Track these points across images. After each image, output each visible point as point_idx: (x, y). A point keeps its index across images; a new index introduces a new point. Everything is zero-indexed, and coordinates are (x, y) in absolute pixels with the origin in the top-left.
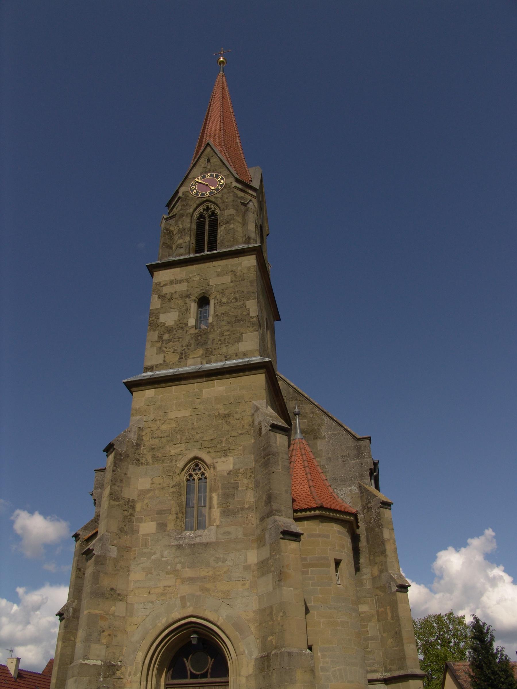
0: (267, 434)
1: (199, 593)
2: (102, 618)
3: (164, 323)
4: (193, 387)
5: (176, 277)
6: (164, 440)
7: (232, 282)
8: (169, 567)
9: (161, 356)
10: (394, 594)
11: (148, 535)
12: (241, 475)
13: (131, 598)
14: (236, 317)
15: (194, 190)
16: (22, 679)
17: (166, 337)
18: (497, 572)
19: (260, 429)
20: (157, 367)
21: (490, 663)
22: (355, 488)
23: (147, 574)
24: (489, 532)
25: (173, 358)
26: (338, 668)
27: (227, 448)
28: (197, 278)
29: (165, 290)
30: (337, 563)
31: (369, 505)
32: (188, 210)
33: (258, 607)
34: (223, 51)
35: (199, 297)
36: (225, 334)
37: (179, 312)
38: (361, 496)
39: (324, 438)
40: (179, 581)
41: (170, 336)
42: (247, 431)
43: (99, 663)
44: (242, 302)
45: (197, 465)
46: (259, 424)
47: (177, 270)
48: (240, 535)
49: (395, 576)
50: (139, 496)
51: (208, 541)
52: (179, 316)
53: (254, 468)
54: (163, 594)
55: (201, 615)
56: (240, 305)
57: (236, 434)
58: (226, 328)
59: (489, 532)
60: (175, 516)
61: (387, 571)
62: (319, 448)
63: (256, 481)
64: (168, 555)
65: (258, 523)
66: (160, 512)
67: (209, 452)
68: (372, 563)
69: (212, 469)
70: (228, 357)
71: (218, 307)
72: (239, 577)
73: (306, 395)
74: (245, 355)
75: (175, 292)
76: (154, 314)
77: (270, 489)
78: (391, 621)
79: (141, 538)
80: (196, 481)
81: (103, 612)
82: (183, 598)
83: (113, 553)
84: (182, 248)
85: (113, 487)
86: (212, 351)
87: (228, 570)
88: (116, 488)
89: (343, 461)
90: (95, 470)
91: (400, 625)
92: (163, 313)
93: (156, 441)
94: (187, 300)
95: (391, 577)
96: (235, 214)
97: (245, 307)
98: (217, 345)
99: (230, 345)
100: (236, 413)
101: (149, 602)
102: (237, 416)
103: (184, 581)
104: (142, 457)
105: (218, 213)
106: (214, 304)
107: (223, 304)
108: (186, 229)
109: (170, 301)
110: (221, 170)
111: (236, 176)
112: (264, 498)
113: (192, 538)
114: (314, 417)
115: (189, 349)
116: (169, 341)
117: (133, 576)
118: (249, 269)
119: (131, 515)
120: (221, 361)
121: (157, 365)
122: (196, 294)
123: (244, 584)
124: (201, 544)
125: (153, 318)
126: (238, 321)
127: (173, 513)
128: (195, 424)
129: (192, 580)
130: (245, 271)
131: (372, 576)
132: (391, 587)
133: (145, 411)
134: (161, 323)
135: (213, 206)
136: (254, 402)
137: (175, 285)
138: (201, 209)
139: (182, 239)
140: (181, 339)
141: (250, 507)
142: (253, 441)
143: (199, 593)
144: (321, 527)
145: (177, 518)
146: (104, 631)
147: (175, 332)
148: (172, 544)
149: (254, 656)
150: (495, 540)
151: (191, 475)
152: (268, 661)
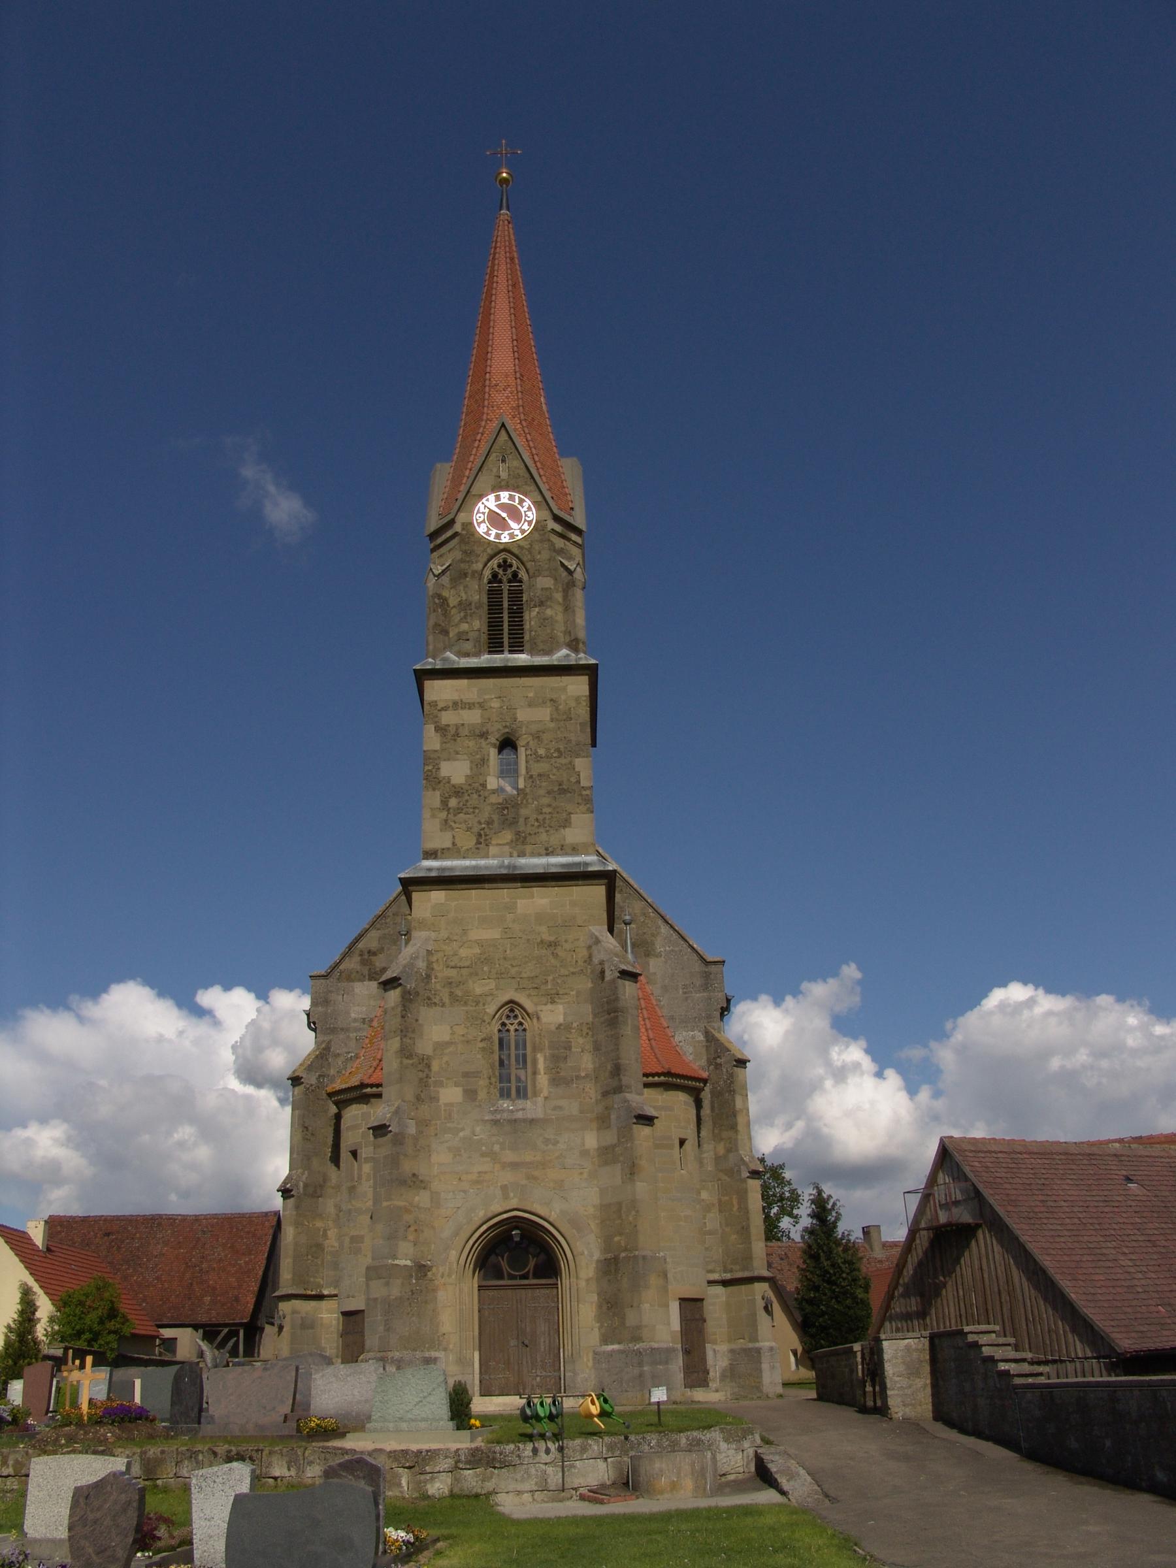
0: (613, 981)
1: (524, 1182)
2: (408, 1211)
3: (449, 778)
4: (504, 894)
5: (462, 697)
6: (465, 972)
7: (552, 720)
8: (484, 1148)
9: (448, 835)
10: (744, 1181)
11: (451, 1105)
12: (574, 1031)
13: (435, 1185)
14: (560, 785)
15: (481, 522)
16: (1031, 1288)
17: (453, 802)
18: (854, 1053)
19: (603, 972)
20: (443, 853)
21: (831, 1252)
22: (700, 1034)
23: (455, 1156)
24: (851, 971)
25: (467, 841)
26: (679, 1269)
27: (554, 992)
28: (496, 704)
29: (447, 718)
30: (682, 1142)
31: (718, 1061)
32: (474, 565)
33: (599, 1201)
34: (506, 150)
35: (500, 740)
36: (544, 810)
37: (471, 762)
38: (707, 1046)
39: (659, 955)
40: (497, 1166)
41: (459, 803)
42: (582, 970)
43: (409, 1263)
44: (569, 759)
45: (512, 1011)
46: (600, 964)
47: (463, 683)
48: (575, 1111)
49: (746, 1159)
50: (434, 1050)
51: (534, 1116)
52: (471, 769)
53: (593, 1023)
54: (477, 1182)
55: (529, 1208)
56: (565, 765)
57: (567, 973)
58: (546, 801)
59: (851, 971)
60: (487, 1081)
61: (737, 1150)
62: (652, 970)
63: (595, 1042)
64: (482, 1133)
65: (599, 1097)
66: (466, 1075)
67: (529, 996)
68: (717, 1138)
69: (535, 1020)
70: (550, 849)
71: (531, 762)
72: (575, 1164)
73: (635, 886)
74: (575, 850)
75: (463, 725)
76: (430, 759)
77: (619, 1058)
78: (738, 1214)
79: (443, 1109)
80: (512, 1033)
81: (407, 1204)
82: (504, 1188)
83: (412, 1129)
84: (468, 640)
85: (404, 1040)
86: (525, 838)
87: (561, 1154)
88: (409, 1041)
89: (685, 993)
90: (310, 977)
91: (748, 1219)
92: (445, 760)
93: (453, 973)
94: (483, 742)
95: (742, 1159)
96: (552, 587)
97: (574, 769)
98: (533, 828)
99: (552, 831)
100: (566, 941)
101: (460, 1191)
102: (567, 946)
103: (504, 1166)
104: (435, 994)
105: (524, 578)
106: (526, 755)
107: (539, 759)
108: (473, 604)
109: (455, 740)
110: (528, 488)
111: (556, 511)
112: (609, 1068)
113: (512, 1111)
114: (646, 921)
115: (491, 829)
116: (459, 810)
117: (435, 1158)
118: (577, 699)
119: (428, 1076)
120: (540, 855)
121: (443, 849)
122: (496, 733)
123: (581, 1173)
124: (524, 1120)
125: (430, 768)
126: (563, 791)
127: (485, 1076)
128: (508, 952)
129: (515, 1166)
130: (573, 704)
131: (716, 1154)
132: (740, 1172)
133: (433, 924)
134: (444, 778)
135: (514, 562)
136: (590, 928)
137: (461, 712)
138: (494, 563)
139: (467, 622)
140: (477, 811)
141: (587, 1076)
142: (590, 985)
143: (524, 1182)
144: (664, 1096)
145: (491, 1084)
146: (409, 1226)
147: (467, 797)
148: (486, 1118)
149: (595, 1258)
150: (858, 989)
151: (504, 1024)
152: (616, 1265)
